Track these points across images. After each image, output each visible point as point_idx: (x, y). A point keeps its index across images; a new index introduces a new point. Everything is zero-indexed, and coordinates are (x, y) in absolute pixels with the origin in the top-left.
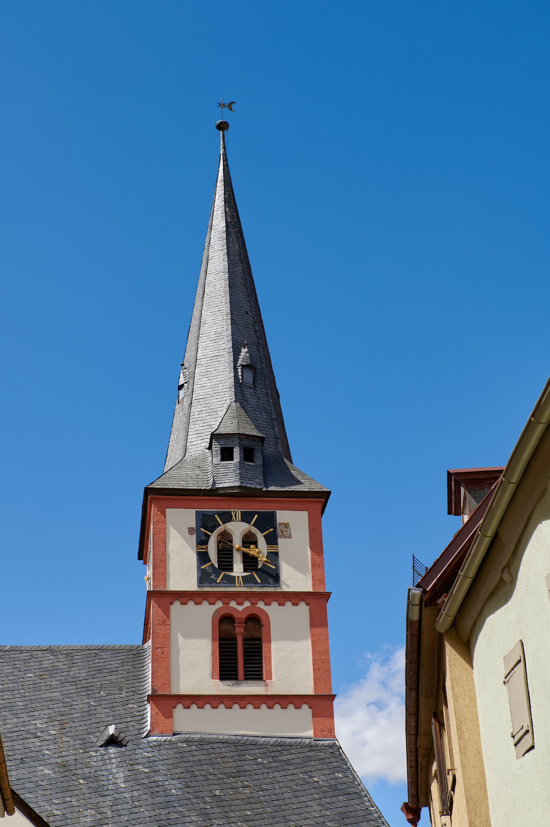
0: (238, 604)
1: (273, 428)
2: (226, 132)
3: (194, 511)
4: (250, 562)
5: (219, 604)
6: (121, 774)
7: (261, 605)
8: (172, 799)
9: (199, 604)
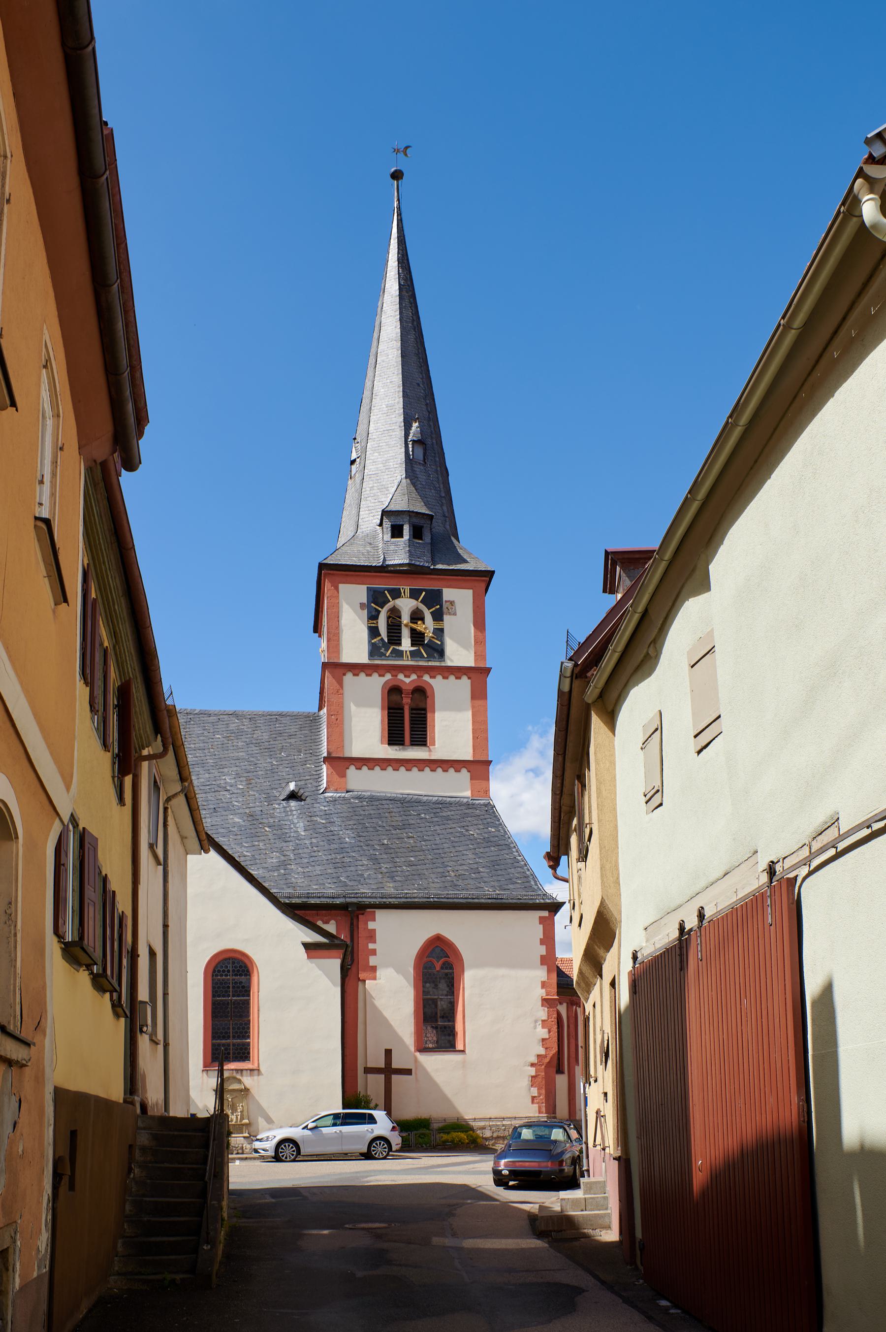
0: (405, 676)
3: (365, 586)
4: (417, 637)
5: (388, 676)
7: (426, 678)
8: (346, 846)
9: (370, 675)
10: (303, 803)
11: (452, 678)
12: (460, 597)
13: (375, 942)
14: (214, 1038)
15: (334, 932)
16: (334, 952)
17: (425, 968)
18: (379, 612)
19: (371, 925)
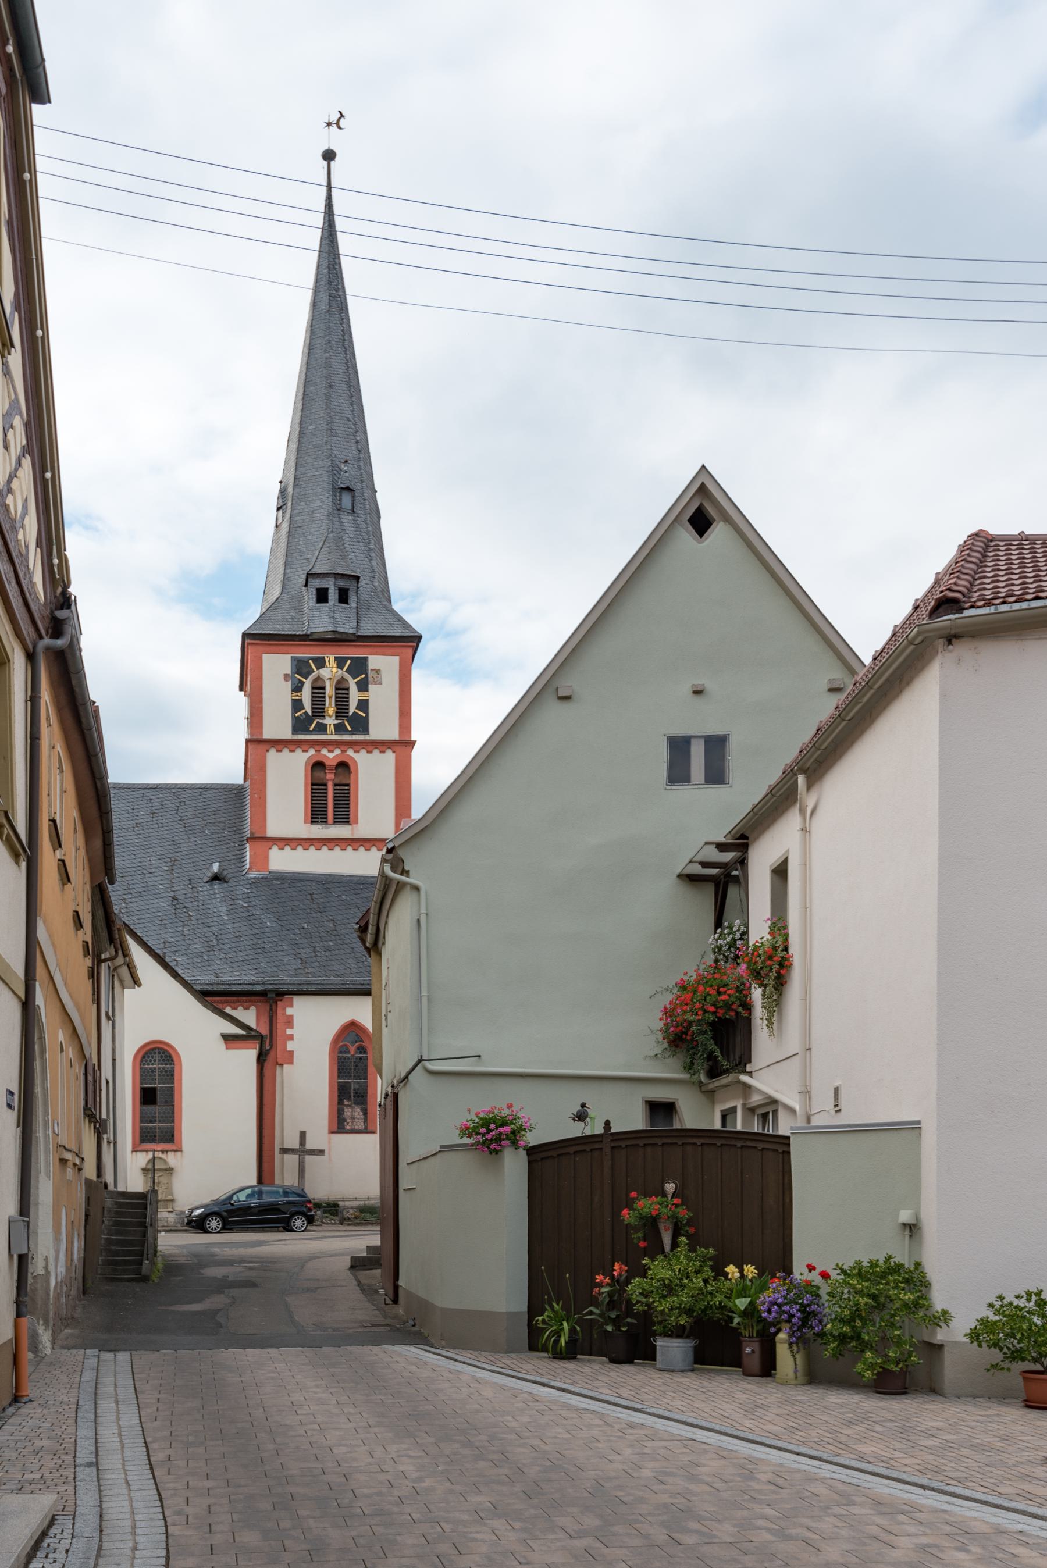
0: (329, 751)
1: (371, 559)
2: (332, 163)
3: (289, 656)
4: (341, 709)
5: (312, 752)
6: (225, 908)
7: (350, 752)
8: (267, 930)
9: (293, 751)
10: (225, 885)
11: (376, 752)
12: (383, 663)
13: (292, 1027)
14: (142, 1121)
15: (253, 1025)
16: (250, 1043)
17: (341, 1052)
18: (303, 683)
19: (289, 1011)
